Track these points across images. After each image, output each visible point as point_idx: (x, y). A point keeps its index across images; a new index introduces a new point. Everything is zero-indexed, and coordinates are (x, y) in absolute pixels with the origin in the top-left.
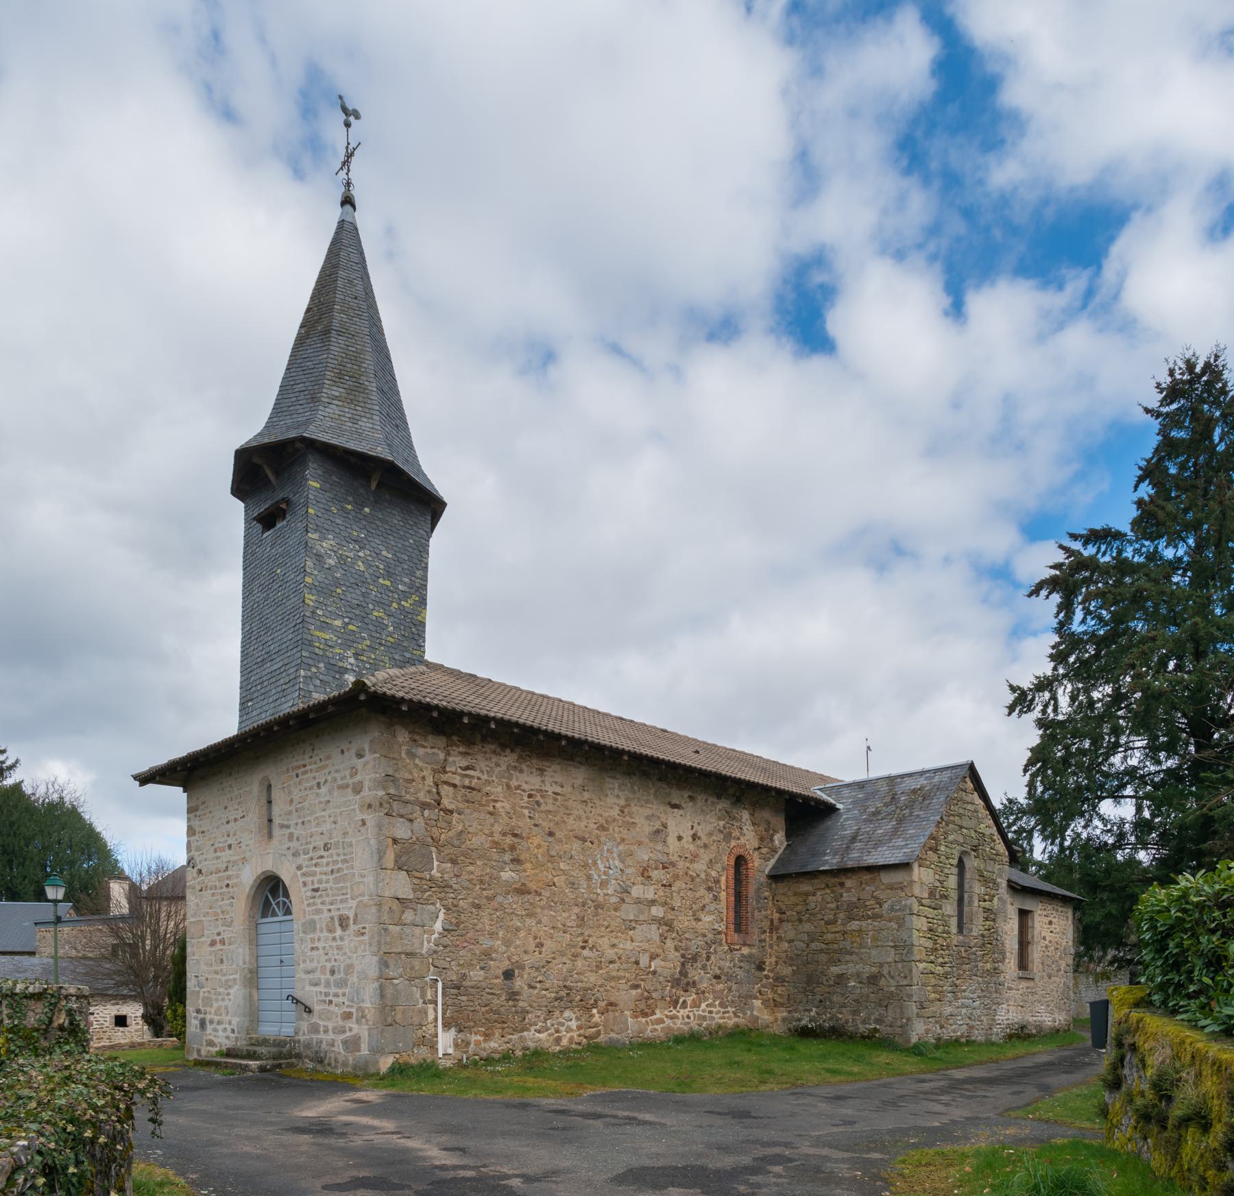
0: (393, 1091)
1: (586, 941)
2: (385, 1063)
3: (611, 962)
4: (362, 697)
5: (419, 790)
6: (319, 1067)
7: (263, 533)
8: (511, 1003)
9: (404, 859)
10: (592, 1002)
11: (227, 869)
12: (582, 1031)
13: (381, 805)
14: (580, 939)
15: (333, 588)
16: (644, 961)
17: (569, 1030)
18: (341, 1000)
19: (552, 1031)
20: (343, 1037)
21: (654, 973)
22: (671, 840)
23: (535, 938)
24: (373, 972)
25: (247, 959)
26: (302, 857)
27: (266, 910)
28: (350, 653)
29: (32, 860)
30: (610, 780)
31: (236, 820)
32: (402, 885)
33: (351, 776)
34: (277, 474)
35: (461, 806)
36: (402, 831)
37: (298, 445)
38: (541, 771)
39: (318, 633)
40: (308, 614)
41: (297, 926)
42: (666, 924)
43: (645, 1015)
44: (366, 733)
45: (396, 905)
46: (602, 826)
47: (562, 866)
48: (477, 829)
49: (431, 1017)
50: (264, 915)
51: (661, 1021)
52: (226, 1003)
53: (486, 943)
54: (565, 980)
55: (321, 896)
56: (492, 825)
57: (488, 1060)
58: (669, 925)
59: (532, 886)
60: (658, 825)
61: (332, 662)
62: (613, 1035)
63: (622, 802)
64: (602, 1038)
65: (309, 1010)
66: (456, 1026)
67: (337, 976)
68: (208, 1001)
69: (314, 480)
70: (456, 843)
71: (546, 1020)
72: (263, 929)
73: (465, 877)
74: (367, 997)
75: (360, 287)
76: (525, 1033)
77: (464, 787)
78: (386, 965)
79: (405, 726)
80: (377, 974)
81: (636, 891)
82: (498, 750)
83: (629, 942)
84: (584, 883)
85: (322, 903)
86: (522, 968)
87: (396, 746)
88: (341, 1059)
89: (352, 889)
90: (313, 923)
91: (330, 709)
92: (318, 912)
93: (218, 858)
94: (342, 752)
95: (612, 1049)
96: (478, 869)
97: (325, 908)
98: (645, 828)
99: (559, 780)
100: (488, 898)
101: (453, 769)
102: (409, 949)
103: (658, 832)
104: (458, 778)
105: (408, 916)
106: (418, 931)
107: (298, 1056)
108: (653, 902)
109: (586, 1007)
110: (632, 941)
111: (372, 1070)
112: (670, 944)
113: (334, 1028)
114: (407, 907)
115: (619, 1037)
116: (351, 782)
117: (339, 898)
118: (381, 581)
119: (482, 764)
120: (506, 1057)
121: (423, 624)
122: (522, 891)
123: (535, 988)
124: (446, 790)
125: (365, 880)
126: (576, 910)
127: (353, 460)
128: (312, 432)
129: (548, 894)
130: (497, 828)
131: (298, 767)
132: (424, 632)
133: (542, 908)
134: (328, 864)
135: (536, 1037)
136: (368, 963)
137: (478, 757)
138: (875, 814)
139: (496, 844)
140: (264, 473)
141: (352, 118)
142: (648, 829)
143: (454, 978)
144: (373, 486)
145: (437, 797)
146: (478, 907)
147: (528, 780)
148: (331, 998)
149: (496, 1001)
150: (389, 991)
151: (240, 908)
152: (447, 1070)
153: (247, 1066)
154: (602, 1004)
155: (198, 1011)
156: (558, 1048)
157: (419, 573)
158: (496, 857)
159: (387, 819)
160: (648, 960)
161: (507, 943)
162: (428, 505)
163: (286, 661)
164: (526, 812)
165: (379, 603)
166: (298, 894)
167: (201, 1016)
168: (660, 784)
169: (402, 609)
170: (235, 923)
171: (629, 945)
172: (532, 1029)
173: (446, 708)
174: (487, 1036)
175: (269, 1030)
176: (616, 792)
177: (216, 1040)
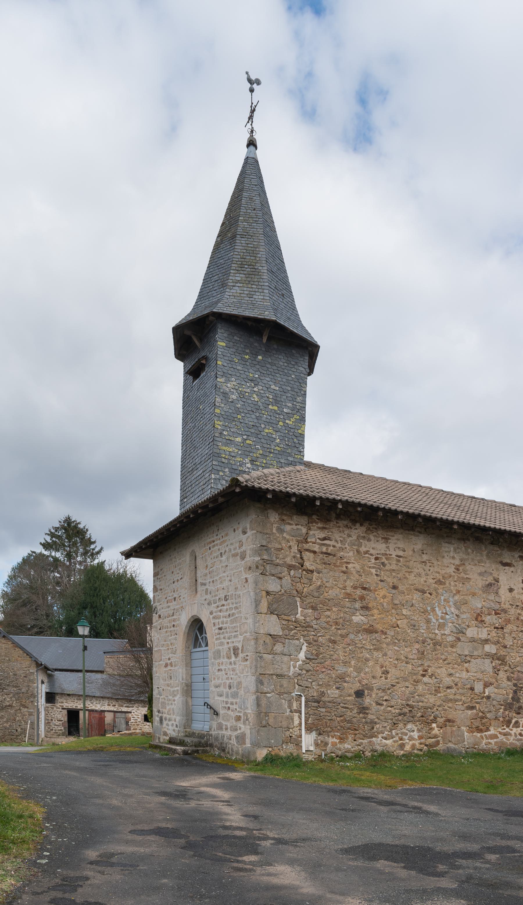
0: (252, 774)
2: (261, 754)
3: (448, 688)
4: (238, 490)
5: (287, 556)
6: (222, 754)
7: (193, 382)
8: (361, 715)
9: (275, 606)
10: (432, 718)
11: (173, 615)
12: (423, 741)
13: (257, 567)
14: (420, 668)
15: (235, 416)
16: (479, 687)
17: (411, 739)
18: (235, 707)
19: (397, 738)
20: (236, 733)
21: (488, 697)
22: (503, 592)
23: (382, 667)
24: (252, 688)
25: (184, 677)
26: (213, 605)
27: (196, 643)
28: (247, 460)
29: (107, 611)
30: (447, 545)
31: (178, 581)
32: (273, 625)
33: (240, 548)
34: (201, 340)
35: (320, 567)
36: (273, 586)
37: (211, 318)
38: (386, 540)
39: (224, 448)
40: (217, 435)
41: (210, 654)
42: (498, 659)
43: (480, 731)
44: (248, 516)
45: (268, 640)
46: (439, 580)
47: (404, 612)
48: (333, 585)
49: (296, 722)
50: (195, 647)
51: (495, 736)
52: (173, 706)
53: (341, 669)
54: (408, 700)
55: (223, 633)
56: (345, 581)
57: (343, 758)
58: (502, 660)
59: (379, 627)
60: (490, 579)
61: (234, 467)
62: (450, 745)
63: (457, 562)
64: (441, 747)
65: (216, 713)
66: (317, 730)
67: (233, 690)
68: (164, 705)
69: (222, 342)
70: (316, 594)
71: (391, 730)
72: (195, 656)
73: (323, 619)
74: (249, 706)
75: (258, 202)
77: (322, 553)
78: (262, 683)
79: (276, 510)
80: (255, 689)
81: (471, 632)
82: (350, 524)
83: (464, 673)
84: (423, 625)
85: (224, 638)
86: (371, 689)
87: (268, 525)
88: (235, 749)
89: (240, 628)
90: (219, 652)
91: (221, 500)
92: (222, 644)
93: (169, 607)
94: (234, 530)
95: (449, 756)
96: (333, 614)
97: (225, 641)
98: (478, 582)
99: (401, 546)
101: (313, 540)
102: (279, 672)
103: (490, 585)
104: (317, 546)
105: (278, 648)
106: (286, 659)
107: (211, 745)
108: (486, 641)
109: (426, 721)
110: (468, 671)
111: (252, 759)
112: (502, 675)
113: (231, 727)
114: (278, 641)
115: (456, 747)
116: (239, 551)
117: (233, 634)
118: (270, 407)
119: (337, 536)
120: (358, 756)
121: (302, 436)
122: (370, 631)
123: (382, 705)
124: (307, 555)
125: (248, 621)
126: (417, 646)
127: (249, 323)
128: (221, 308)
129: (392, 633)
131: (210, 543)
132: (303, 441)
133: (388, 644)
134: (227, 610)
135: (382, 742)
136: (249, 681)
137: (334, 530)
139: (348, 595)
140: (192, 339)
141: (255, 86)
143: (315, 694)
144: (265, 340)
145: (300, 561)
146: (334, 642)
147: (375, 546)
148: (229, 705)
149: (349, 713)
150: (264, 702)
151: (179, 641)
152: (308, 762)
153: (175, 750)
154: (441, 720)
155: (159, 712)
156: (402, 752)
157: (299, 399)
158: (348, 605)
159: (261, 578)
160: (482, 687)
161: (359, 670)
162: (306, 350)
163: (204, 469)
164: (373, 571)
165: (269, 423)
166: (210, 631)
167: (160, 715)
168: (491, 547)
169: (286, 426)
170: (178, 652)
171: (464, 675)
172: (380, 736)
173: (301, 495)
174: (342, 740)
175: (198, 727)
176: (452, 554)
177: (168, 732)
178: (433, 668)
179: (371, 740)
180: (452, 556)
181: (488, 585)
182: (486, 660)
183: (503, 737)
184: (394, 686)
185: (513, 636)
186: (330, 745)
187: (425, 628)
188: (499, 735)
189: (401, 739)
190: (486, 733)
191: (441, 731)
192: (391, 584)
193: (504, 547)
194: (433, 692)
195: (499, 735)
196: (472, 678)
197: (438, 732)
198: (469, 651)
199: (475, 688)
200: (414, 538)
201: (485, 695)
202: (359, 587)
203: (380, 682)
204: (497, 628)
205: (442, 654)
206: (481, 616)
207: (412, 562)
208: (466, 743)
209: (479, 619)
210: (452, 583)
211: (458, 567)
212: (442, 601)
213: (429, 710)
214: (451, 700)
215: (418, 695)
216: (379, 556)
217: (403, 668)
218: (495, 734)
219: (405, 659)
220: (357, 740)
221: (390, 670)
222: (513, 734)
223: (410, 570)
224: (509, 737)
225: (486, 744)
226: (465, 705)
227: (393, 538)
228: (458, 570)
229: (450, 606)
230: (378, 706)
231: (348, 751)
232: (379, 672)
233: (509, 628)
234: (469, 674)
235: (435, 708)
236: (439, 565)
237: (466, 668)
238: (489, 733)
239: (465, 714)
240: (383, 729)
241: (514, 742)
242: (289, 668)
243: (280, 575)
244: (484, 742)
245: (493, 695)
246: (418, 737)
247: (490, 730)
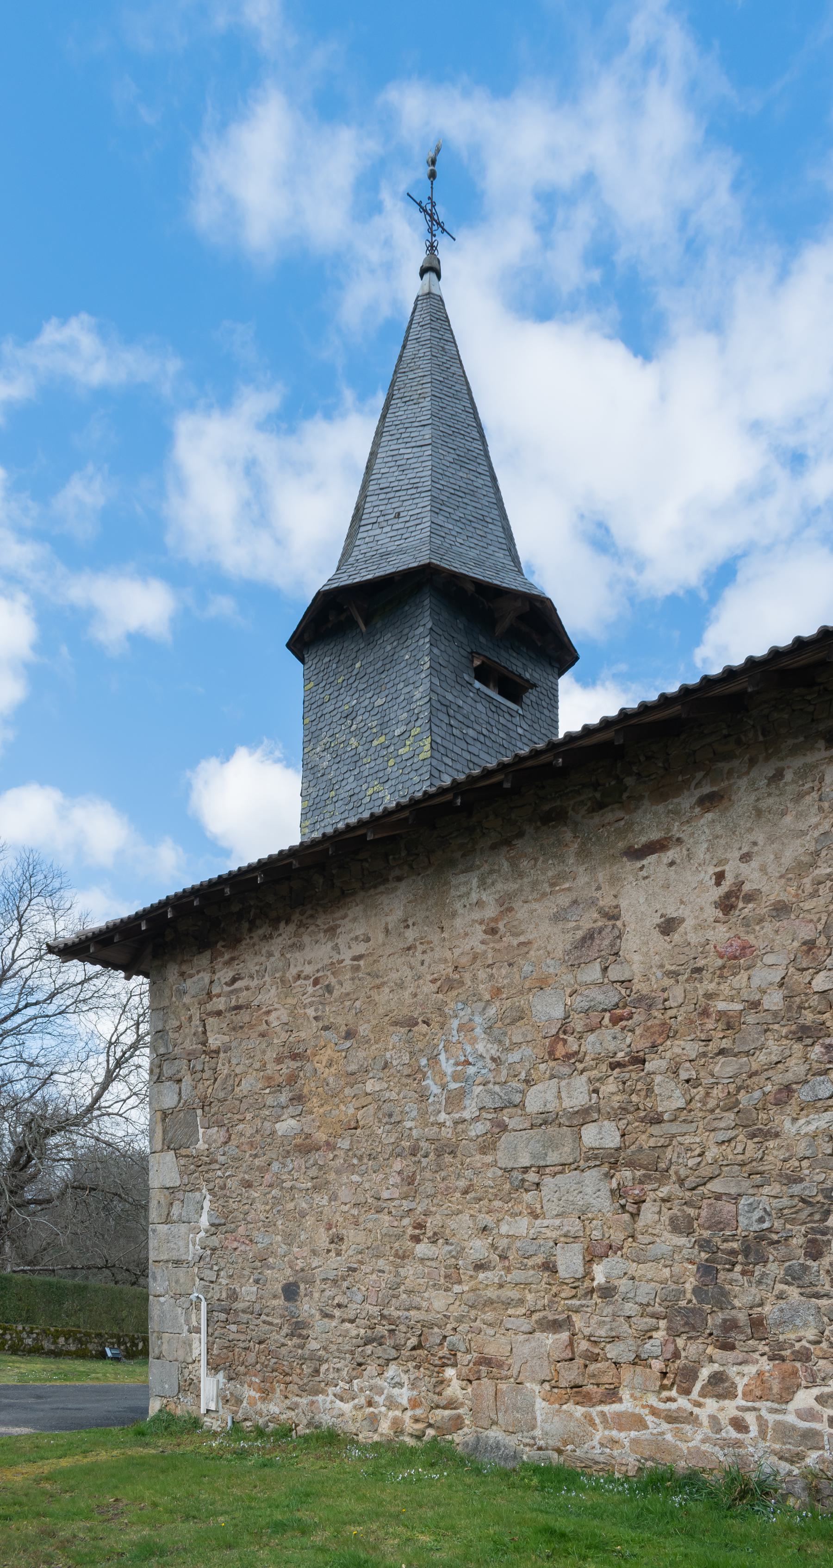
1: (420, 1226)
8: (296, 1340)
14: (406, 1221)
16: (570, 1261)
17: (391, 1404)
19: (361, 1400)
21: (607, 1292)
30: (462, 878)
43: (586, 1399)
53: (262, 1240)
56: (264, 1052)
59: (321, 1136)
60: (589, 920)
63: (490, 911)
76: (320, 1398)
81: (539, 1098)
84: (413, 1109)
99: (360, 931)
100: (261, 1169)
102: (175, 1256)
103: (589, 937)
106: (183, 1228)
108: (584, 1116)
123: (331, 1317)
126: (398, 1165)
130: (271, 1055)
132: (557, 702)
133: (338, 1172)
135: (336, 1408)
138: (260, 1343)
142: (560, 940)
149: (275, 1336)
161: (289, 1238)
172: (331, 1390)
174: (266, 1394)
178: (438, 1217)
179: (315, 1398)
180: (475, 901)
181: (584, 939)
182: (588, 1173)
183: (665, 1426)
184: (354, 1270)
185: (684, 1075)
186: (245, 1404)
187: (414, 1114)
188: (650, 1419)
189: (370, 1404)
190: (606, 1408)
191: (469, 1390)
192: (343, 1028)
193: (641, 798)
194: (442, 1281)
195: (650, 1419)
196: (549, 1234)
197: (460, 1394)
198: (533, 1156)
199: (559, 1263)
200: (384, 899)
201: (595, 1284)
202: (286, 1057)
203: (334, 1264)
204: (619, 1065)
205: (459, 1177)
206: (565, 1041)
207: (383, 960)
208: (537, 1432)
209: (560, 1051)
210: (482, 975)
211: (493, 925)
212: (455, 1032)
213: (436, 1330)
214: (491, 1302)
215: (405, 1292)
216: (320, 974)
217: (370, 1225)
218: (633, 1415)
219: (375, 1202)
220: (290, 1395)
221: (344, 1232)
222: (705, 1421)
223: (378, 981)
224: (687, 1427)
225: (602, 1445)
226: (536, 1317)
227: (347, 920)
228: (493, 931)
229: (474, 1041)
230: (326, 1320)
231: (274, 1419)
232: (323, 1239)
233: (668, 1055)
234: (538, 1222)
235: (449, 1327)
236: (444, 939)
237: (528, 1206)
238: (616, 1407)
239: (533, 1344)
240: (336, 1375)
241: (705, 1447)
242: (187, 1247)
243: (178, 1077)
244: (598, 1436)
245: (623, 1285)
246: (410, 1400)
247: (620, 1400)
